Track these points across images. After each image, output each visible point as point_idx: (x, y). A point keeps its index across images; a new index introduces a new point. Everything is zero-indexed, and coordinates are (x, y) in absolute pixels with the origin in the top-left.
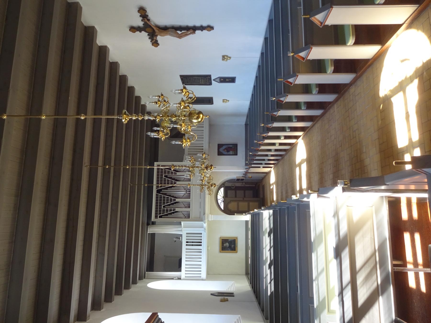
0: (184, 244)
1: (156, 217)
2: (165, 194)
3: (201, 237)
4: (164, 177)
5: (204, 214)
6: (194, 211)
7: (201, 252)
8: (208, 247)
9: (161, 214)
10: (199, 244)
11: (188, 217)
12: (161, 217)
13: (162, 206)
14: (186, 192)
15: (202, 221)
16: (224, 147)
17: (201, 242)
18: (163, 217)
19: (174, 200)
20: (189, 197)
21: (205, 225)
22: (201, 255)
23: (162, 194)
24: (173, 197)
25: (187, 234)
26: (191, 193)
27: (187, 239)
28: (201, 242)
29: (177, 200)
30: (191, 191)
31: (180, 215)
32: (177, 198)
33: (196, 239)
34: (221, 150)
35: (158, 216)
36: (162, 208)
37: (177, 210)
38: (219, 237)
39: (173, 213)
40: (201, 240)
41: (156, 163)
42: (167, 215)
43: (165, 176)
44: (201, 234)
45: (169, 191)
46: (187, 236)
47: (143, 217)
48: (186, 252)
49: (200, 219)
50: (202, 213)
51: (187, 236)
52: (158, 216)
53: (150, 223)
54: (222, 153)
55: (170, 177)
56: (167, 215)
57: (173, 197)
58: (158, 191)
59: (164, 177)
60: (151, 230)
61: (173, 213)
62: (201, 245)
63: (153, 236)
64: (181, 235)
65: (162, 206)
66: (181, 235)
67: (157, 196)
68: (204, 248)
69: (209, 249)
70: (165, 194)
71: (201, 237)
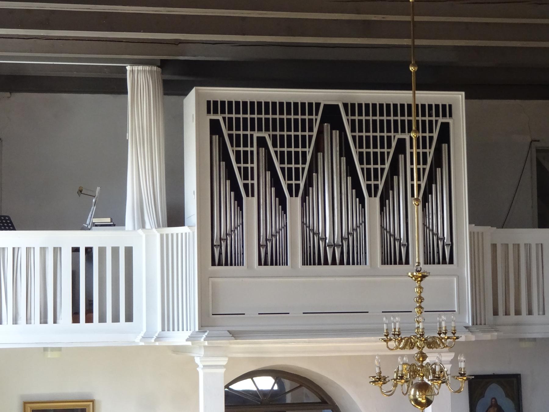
0: (81, 238)
1: (213, 106)
2: (319, 147)
3: (116, 319)
4: (399, 136)
5: (235, 335)
6: (250, 285)
7: (44, 321)
8: (59, 349)
9: (226, 132)
10: (83, 309)
11: (221, 254)
12: (215, 127)
13: (263, 134)
14: (333, 246)
15: (203, 326)
16: (507, 404)
17: (89, 319)
18: (216, 138)
19: (294, 190)
20: (311, 258)
21: (179, 338)
22: (28, 321)
23: (320, 132)
24: (309, 183)
25: (129, 251)
26: (330, 268)
27: (102, 251)
28: (89, 319)
29: (294, 204)
30: (337, 268)
31: (226, 220)
32: (303, 200)
33: (105, 296)
34: (495, 392)
35: (219, 117)
36: (256, 134)
37: (250, 204)
38: (96, 398)
39: (235, 187)
40: (102, 319)
41: (457, 99)
42: (224, 156)
43: (401, 142)
44: (129, 318)
45: (332, 164)
46: (115, 251)
47: (201, 45)
48: (43, 250)
49: (211, 317)
50: (236, 324)
51: (115, 251)
52: (219, 117)
53: (177, 77)
54: (482, 395)
55: (379, 163)
56: (224, 156)
57: (309, 183)
58: (331, 114)
59: (399, 136)
60: (140, 80)
61: (235, 187)
62: (76, 318)
63: (116, 85)
64: (117, 222)
65: (263, 134)
66: (117, 222)
67: (311, 107)
68: (65, 333)
69: (50, 355)
70: (319, 147)
71: (116, 319)
